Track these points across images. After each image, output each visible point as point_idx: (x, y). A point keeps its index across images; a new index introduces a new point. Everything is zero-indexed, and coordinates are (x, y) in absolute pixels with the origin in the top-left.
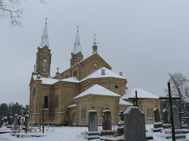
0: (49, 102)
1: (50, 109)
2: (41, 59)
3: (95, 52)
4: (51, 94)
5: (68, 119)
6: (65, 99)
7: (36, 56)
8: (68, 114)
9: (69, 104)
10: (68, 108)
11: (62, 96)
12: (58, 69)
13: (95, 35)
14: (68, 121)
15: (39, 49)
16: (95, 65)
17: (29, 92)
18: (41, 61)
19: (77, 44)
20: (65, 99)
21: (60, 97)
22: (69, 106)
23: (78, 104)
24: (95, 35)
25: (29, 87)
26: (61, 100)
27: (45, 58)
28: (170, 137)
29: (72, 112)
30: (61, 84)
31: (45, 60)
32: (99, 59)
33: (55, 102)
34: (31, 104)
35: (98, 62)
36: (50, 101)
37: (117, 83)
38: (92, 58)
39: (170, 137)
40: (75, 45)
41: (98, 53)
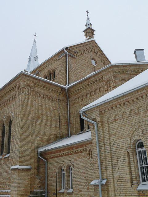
5: (40, 187)
6: (32, 126)
8: (41, 170)
9: (43, 141)
10: (41, 154)
14: (42, 193)
16: (93, 62)
19: (32, 59)
20: (32, 126)
22: (42, 146)
26: (22, 128)
28: (65, 111)
29: (53, 166)
30: (22, 84)
32: (99, 53)
35: (97, 59)
39: (65, 111)
40: (30, 61)
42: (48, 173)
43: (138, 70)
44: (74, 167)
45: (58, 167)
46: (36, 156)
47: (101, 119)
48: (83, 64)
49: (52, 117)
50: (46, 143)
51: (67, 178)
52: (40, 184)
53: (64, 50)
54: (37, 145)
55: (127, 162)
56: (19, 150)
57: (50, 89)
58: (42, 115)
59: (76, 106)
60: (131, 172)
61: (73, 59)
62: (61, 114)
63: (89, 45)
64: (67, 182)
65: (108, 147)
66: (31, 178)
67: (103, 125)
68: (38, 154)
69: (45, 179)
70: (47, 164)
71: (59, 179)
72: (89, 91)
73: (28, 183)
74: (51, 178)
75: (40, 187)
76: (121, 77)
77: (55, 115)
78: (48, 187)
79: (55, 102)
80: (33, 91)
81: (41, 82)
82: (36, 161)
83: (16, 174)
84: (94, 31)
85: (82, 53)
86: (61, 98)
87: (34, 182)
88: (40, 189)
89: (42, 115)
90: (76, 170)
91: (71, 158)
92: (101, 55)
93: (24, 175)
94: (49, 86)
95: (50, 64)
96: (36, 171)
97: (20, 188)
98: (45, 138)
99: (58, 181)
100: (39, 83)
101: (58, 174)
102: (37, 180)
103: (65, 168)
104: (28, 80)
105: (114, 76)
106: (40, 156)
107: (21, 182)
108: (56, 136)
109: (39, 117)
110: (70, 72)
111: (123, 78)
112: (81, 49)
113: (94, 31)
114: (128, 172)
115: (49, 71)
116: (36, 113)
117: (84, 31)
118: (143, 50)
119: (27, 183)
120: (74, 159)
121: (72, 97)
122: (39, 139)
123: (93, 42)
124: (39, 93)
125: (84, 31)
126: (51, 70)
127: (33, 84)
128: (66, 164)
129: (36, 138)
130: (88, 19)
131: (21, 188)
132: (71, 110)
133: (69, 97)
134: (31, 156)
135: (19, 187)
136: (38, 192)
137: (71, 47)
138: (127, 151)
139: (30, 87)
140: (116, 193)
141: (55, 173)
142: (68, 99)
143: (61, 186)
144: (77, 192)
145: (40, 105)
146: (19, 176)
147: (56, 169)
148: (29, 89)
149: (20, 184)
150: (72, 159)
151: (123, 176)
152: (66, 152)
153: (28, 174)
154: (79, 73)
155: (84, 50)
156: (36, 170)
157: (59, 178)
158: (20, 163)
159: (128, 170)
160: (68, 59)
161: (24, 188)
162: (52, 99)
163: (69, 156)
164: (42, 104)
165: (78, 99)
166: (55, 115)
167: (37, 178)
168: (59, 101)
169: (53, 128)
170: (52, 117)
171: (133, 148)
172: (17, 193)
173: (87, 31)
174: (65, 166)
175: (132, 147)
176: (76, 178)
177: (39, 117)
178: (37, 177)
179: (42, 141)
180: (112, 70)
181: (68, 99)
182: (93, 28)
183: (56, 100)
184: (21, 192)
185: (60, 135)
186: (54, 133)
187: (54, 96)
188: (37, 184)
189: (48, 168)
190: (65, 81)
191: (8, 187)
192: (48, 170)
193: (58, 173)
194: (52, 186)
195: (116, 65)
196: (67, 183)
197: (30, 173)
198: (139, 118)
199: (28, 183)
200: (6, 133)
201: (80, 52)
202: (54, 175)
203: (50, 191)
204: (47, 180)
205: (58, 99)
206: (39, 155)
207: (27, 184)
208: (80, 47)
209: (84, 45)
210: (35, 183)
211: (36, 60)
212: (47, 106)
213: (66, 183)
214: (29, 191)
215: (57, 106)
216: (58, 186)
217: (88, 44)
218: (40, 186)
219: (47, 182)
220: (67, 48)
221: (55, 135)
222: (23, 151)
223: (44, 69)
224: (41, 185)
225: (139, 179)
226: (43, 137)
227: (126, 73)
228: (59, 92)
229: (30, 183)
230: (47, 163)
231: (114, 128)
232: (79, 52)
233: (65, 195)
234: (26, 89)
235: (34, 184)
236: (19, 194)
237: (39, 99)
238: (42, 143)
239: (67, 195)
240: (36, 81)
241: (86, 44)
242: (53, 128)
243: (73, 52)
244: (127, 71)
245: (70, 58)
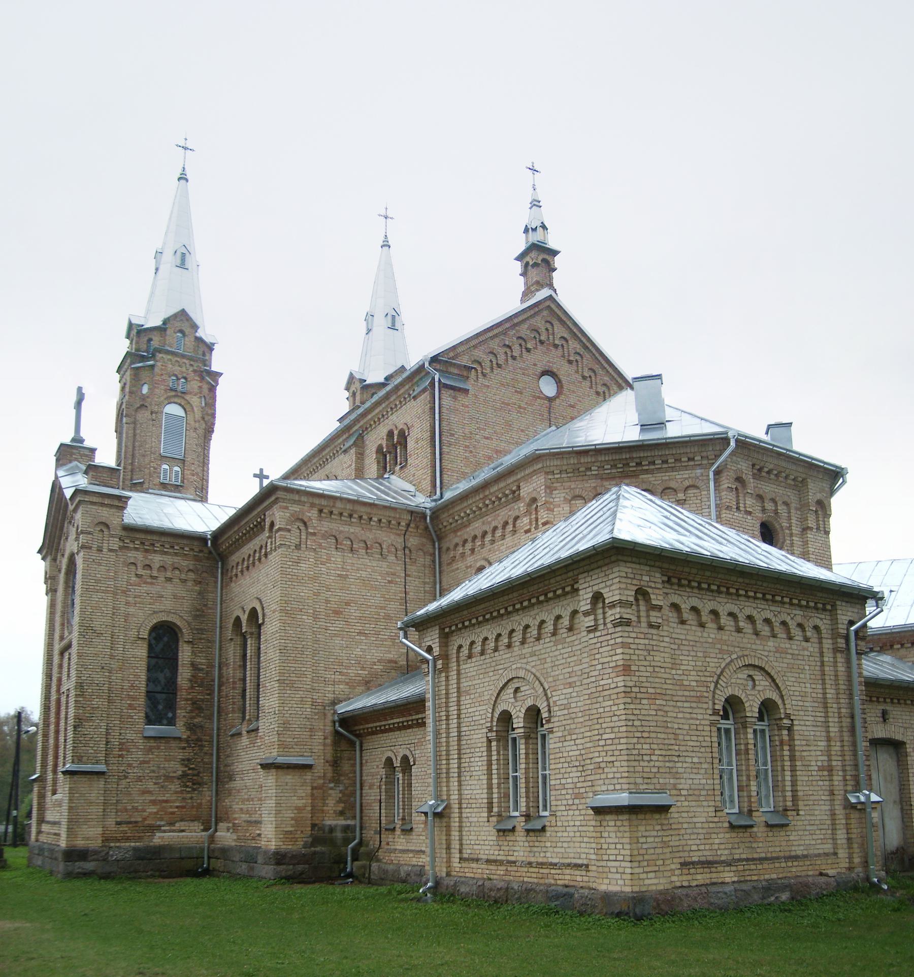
0: (184, 675)
1: (191, 727)
2: (144, 398)
3: (544, 293)
4: (200, 613)
5: (342, 813)
7: (118, 386)
9: (351, 684)
11: (288, 612)
12: (186, 139)
13: (533, 170)
15: (136, 332)
16: (548, 387)
17: (43, 601)
18: (144, 416)
20: (317, 641)
21: (271, 628)
23: (446, 668)
24: (533, 170)
25: (39, 566)
26: (283, 650)
27: (177, 395)
31: (173, 409)
32: (573, 345)
33: (231, 672)
34: (54, 697)
35: (564, 369)
36: (193, 665)
37: (773, 500)
38: (524, 330)
40: (369, 331)
41: (566, 299)
42: (364, 774)
43: (625, 462)
44: (417, 763)
45: (384, 760)
46: (327, 728)
47: (444, 649)
48: (503, 403)
49: (382, 608)
50: (360, 689)
51: (404, 790)
52: (343, 805)
53: (427, 365)
54: (331, 696)
55: (485, 763)
56: (277, 712)
57: (371, 519)
58: (347, 604)
59: (458, 569)
60: (490, 787)
61: (457, 394)
62: (411, 596)
63: (532, 321)
64: (404, 802)
65: (454, 723)
66: (313, 788)
67: (447, 664)
68: (334, 722)
69: (354, 793)
70: (361, 750)
71: (386, 792)
72: (490, 523)
73: (304, 801)
74: (370, 788)
75: (342, 813)
76: (570, 488)
77: (390, 600)
78: (364, 814)
79: (392, 558)
80: (314, 534)
81: (339, 504)
82: (329, 741)
83: (270, 777)
84: (555, 253)
85: (501, 359)
86: (413, 541)
87: (324, 799)
88: (342, 818)
89: (347, 604)
90: (420, 770)
91: (411, 738)
92: (582, 351)
93: (294, 781)
94: (368, 510)
95: (392, 409)
96: (329, 769)
97: (281, 815)
98: (359, 675)
99: (383, 797)
100: (333, 506)
101: (384, 780)
102: (333, 795)
103: (399, 765)
104: (295, 502)
105: (547, 487)
106: (341, 726)
107: (283, 798)
108: (394, 665)
109: (337, 613)
110: (445, 449)
111: (577, 492)
112: (494, 345)
113: (555, 253)
114: (485, 786)
115: (390, 434)
116: (327, 601)
117: (518, 259)
118: (659, 377)
119: (300, 803)
120: (416, 741)
121: (446, 536)
122: (338, 677)
123: (548, 303)
124: (335, 537)
125: (518, 259)
126: (396, 432)
127: (314, 513)
128: (402, 752)
129: (329, 676)
130: (535, 204)
131: (286, 815)
132: (444, 580)
133: (437, 536)
134: (311, 730)
135: (278, 812)
136: (336, 826)
137: (454, 348)
138: (487, 737)
139: (305, 523)
140: (464, 833)
141: (379, 777)
142: (437, 544)
143: (392, 811)
144: (421, 830)
145: (339, 575)
146: (278, 784)
147: (380, 766)
148: (302, 528)
149: (282, 805)
150: (413, 741)
151: (477, 796)
152: (398, 720)
153: (304, 777)
154: (486, 442)
155: (509, 347)
156: (330, 768)
157: (386, 789)
158: (281, 750)
159: (485, 782)
160: (440, 399)
161: (293, 815)
162: (382, 549)
163: (408, 731)
164: (348, 570)
165: (463, 546)
166: (390, 600)
167: (331, 789)
168: (407, 552)
169: (385, 640)
170: (382, 608)
171: (496, 731)
172: (274, 826)
173: (528, 259)
174: (399, 759)
175: (495, 729)
176: (420, 792)
177: (337, 613)
178: (332, 785)
179: (347, 684)
180: (540, 466)
181: (437, 544)
182: (552, 244)
183: (393, 550)
184: (284, 826)
185: (407, 661)
186: (390, 656)
187: (389, 538)
188: (332, 804)
189: (364, 761)
190: (429, 478)
191: (259, 812)
192: (364, 768)
193: (384, 776)
194: (372, 811)
195: (550, 453)
196: (404, 805)
197: (308, 776)
198: (512, 659)
199: (304, 801)
200: (251, 659)
201: (491, 357)
202: (375, 780)
203: (367, 825)
204: (361, 794)
205: (400, 547)
206: (337, 724)
207: (301, 805)
208: (492, 338)
209: (507, 325)
210: (327, 802)
211: (393, 327)
212: (364, 574)
213: (401, 803)
214: (309, 822)
215: (399, 569)
216: (383, 811)
217: (520, 318)
218: (340, 809)
219: (361, 799)
220: (434, 360)
221: (390, 661)
222: (288, 715)
223: (375, 422)
224: (344, 808)
225: (506, 805)
226: (352, 672)
227: (589, 473)
228: (403, 524)
229: (310, 801)
230: (361, 746)
231: (469, 675)
232: (486, 359)
233: (397, 836)
234: (289, 531)
235: (324, 804)
236: (282, 829)
237: (337, 557)
238: (347, 690)
239: (402, 837)
240: (324, 502)
241: (516, 321)
242: (385, 640)
243: (459, 366)
244: (590, 469)
245: (446, 394)
